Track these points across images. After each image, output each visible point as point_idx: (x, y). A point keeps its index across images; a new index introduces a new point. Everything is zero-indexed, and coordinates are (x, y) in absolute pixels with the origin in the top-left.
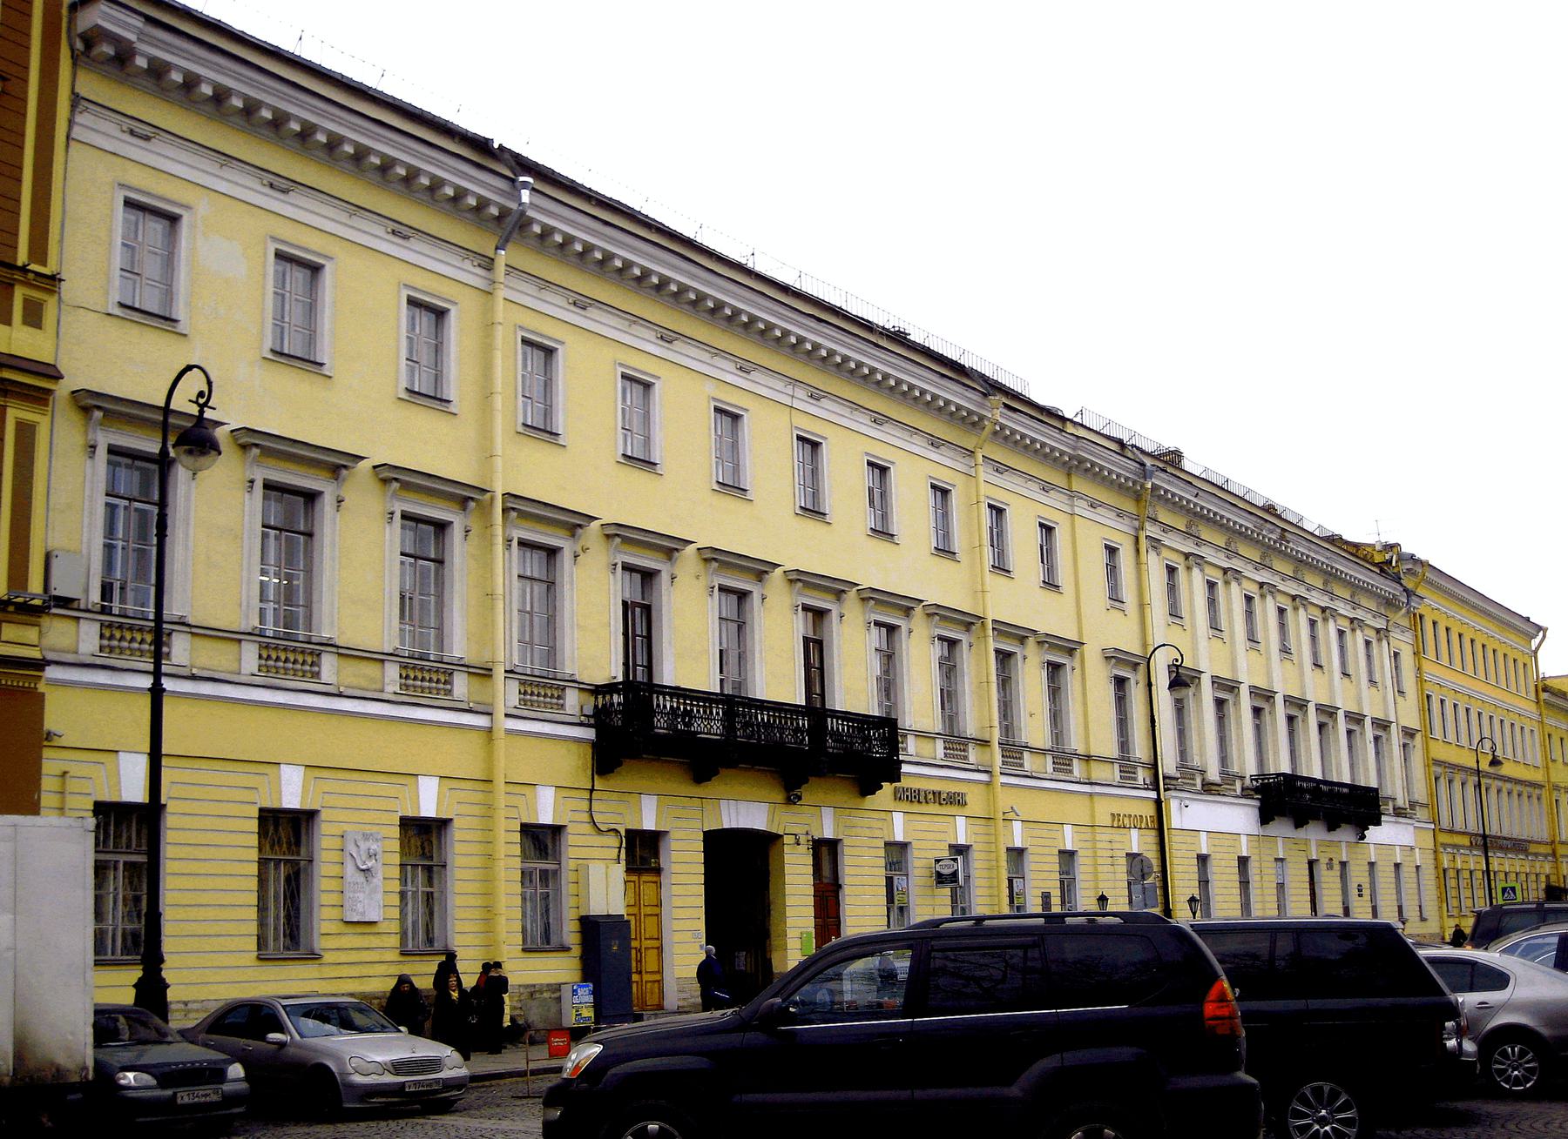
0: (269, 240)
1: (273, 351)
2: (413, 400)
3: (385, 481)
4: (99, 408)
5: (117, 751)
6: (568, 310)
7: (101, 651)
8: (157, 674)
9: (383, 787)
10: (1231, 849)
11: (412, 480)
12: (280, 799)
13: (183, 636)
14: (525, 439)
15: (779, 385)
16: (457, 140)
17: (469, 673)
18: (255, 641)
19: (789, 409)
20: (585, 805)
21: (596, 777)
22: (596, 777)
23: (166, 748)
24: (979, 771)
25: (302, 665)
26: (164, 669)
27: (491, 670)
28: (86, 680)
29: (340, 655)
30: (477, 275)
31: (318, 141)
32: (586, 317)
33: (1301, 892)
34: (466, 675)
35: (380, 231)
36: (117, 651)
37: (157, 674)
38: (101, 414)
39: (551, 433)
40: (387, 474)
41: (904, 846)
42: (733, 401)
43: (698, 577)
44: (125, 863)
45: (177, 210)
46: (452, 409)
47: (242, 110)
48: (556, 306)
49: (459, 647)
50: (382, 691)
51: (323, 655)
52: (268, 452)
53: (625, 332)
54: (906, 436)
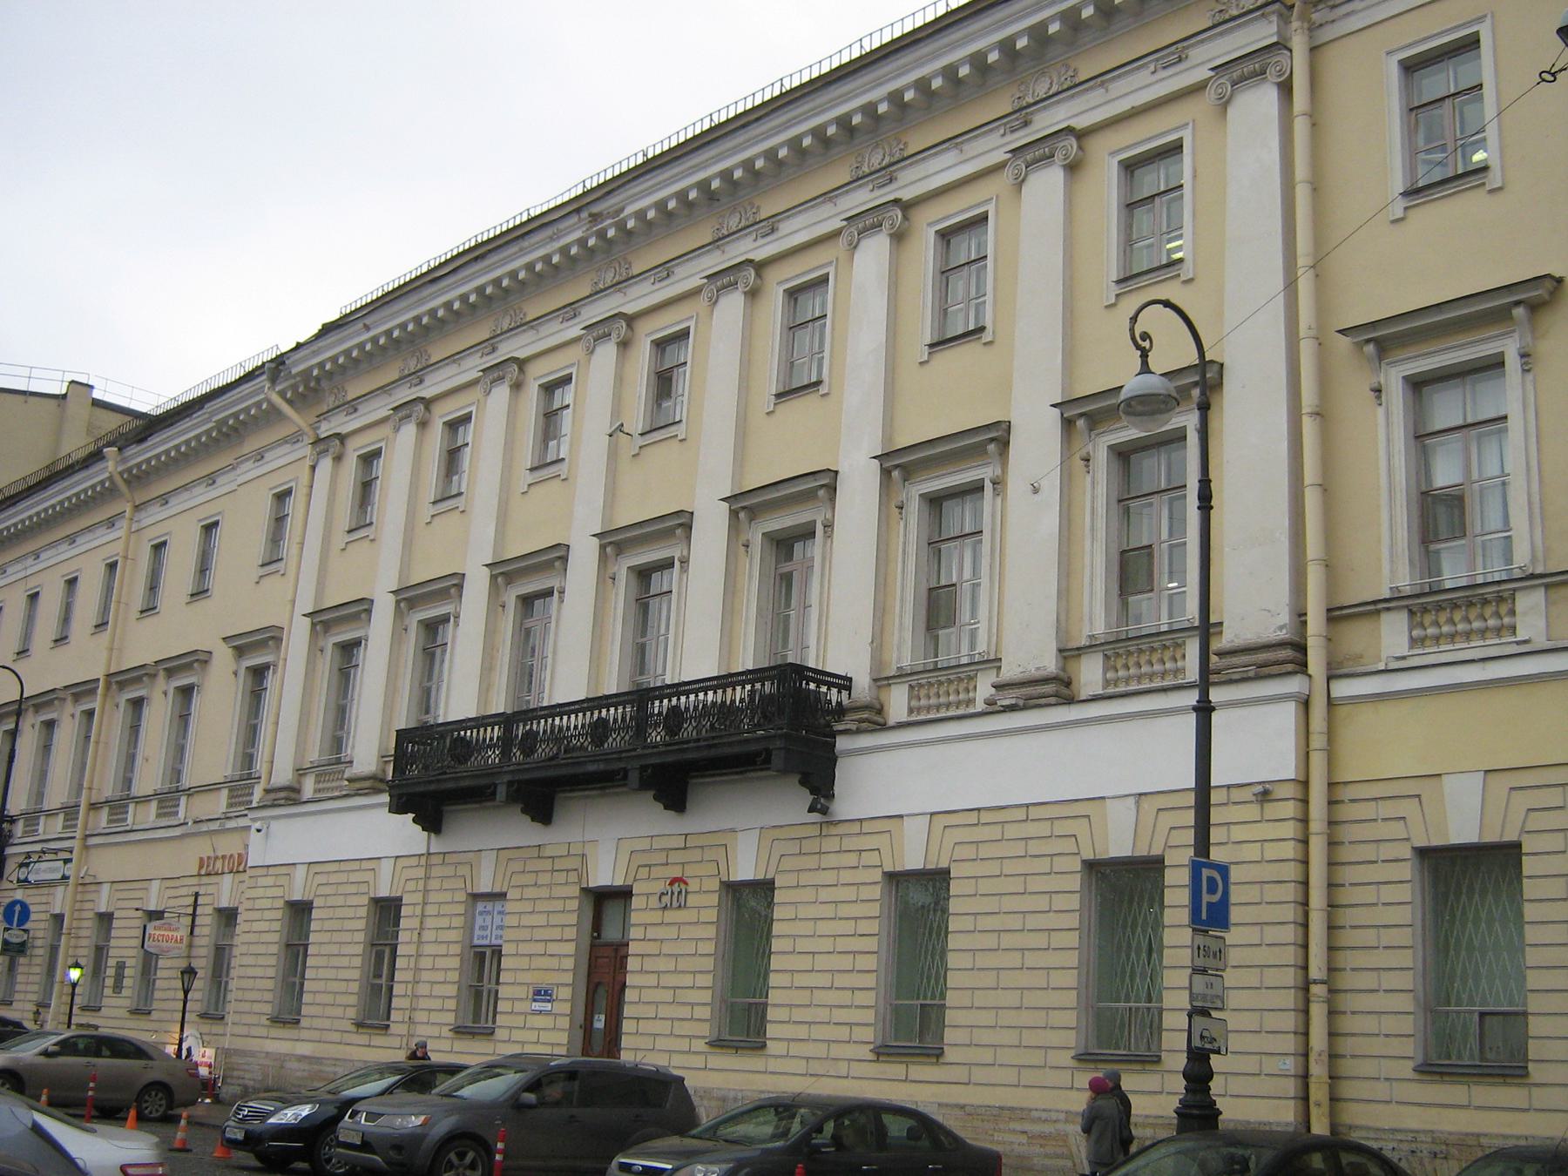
41: (937, 879)
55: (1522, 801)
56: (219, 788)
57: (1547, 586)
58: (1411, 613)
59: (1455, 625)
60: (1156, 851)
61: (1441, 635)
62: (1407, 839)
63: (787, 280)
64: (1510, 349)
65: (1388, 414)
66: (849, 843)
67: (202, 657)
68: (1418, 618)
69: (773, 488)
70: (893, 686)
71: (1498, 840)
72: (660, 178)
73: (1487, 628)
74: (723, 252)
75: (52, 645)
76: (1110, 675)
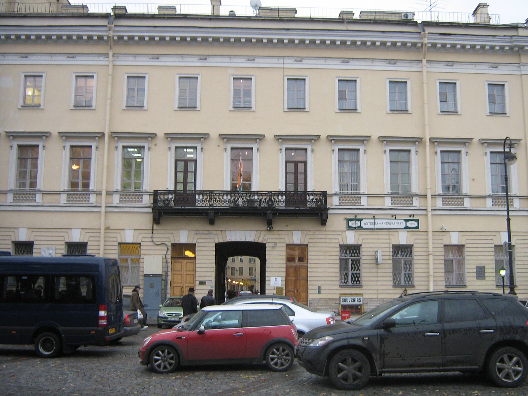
0: (485, 82)
1: (391, 110)
2: (76, 109)
3: (483, 144)
4: (436, 142)
5: (71, 229)
6: (246, 63)
7: (391, 205)
8: (508, 211)
9: (384, 235)
10: (387, 241)
11: (349, 139)
12: (125, 240)
13: (146, 195)
14: (341, 114)
15: (275, 60)
16: (100, 18)
17: (470, 198)
18: (12, 193)
19: (282, 69)
20: (150, 235)
21: (154, 225)
22: (154, 225)
23: (511, 230)
24: (421, 210)
25: (495, 202)
26: (510, 209)
27: (101, 192)
28: (94, 211)
29: (470, 198)
30: (106, 61)
31: (388, 45)
32: (160, 61)
33: (210, 265)
34: (469, 198)
35: (147, 59)
36: (354, 204)
37: (508, 211)
38: (334, 141)
39: (88, 106)
40: (434, 140)
41: (460, 248)
42: (245, 73)
43: (219, 146)
44: (132, 259)
45: (251, 77)
46: (507, 115)
47: (451, 47)
48: (195, 62)
49: (415, 190)
50: (486, 207)
51: (514, 199)
52: (388, 142)
53: (50, 60)
54: (49, 58)
55: (141, 236)
56: (485, 198)
57: (97, 194)
58: (14, 194)
59: (80, 198)
60: (85, 241)
61: (77, 200)
62: (116, 241)
63: (78, 73)
64: (94, 145)
65: (171, 154)
66: (328, 237)
67: (48, 135)
68: (69, 196)
69: (366, 137)
70: (8, 194)
71: (357, 243)
72: (466, 38)
73: (130, 200)
74: (183, 59)
75: (439, 113)
76: (121, 199)
